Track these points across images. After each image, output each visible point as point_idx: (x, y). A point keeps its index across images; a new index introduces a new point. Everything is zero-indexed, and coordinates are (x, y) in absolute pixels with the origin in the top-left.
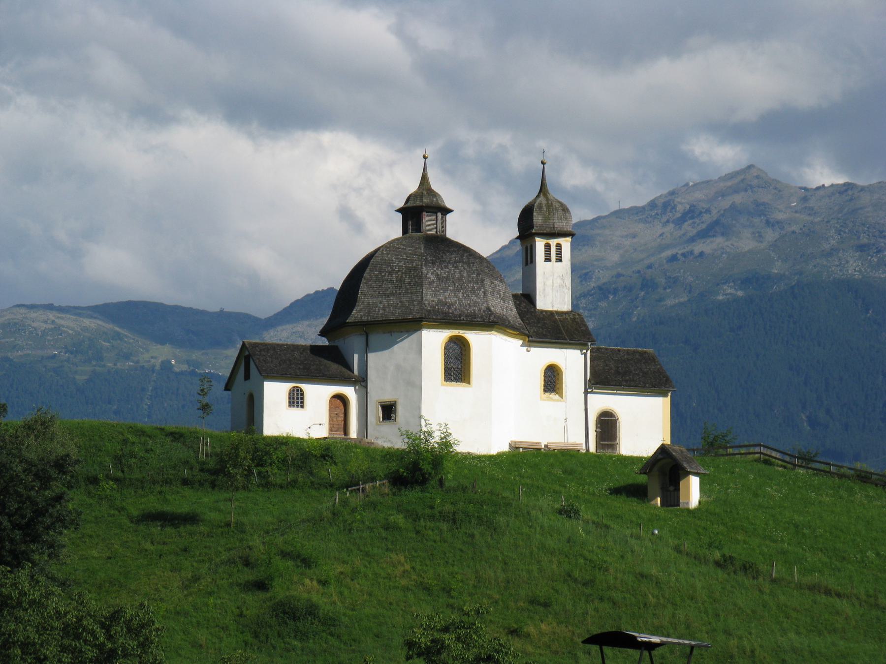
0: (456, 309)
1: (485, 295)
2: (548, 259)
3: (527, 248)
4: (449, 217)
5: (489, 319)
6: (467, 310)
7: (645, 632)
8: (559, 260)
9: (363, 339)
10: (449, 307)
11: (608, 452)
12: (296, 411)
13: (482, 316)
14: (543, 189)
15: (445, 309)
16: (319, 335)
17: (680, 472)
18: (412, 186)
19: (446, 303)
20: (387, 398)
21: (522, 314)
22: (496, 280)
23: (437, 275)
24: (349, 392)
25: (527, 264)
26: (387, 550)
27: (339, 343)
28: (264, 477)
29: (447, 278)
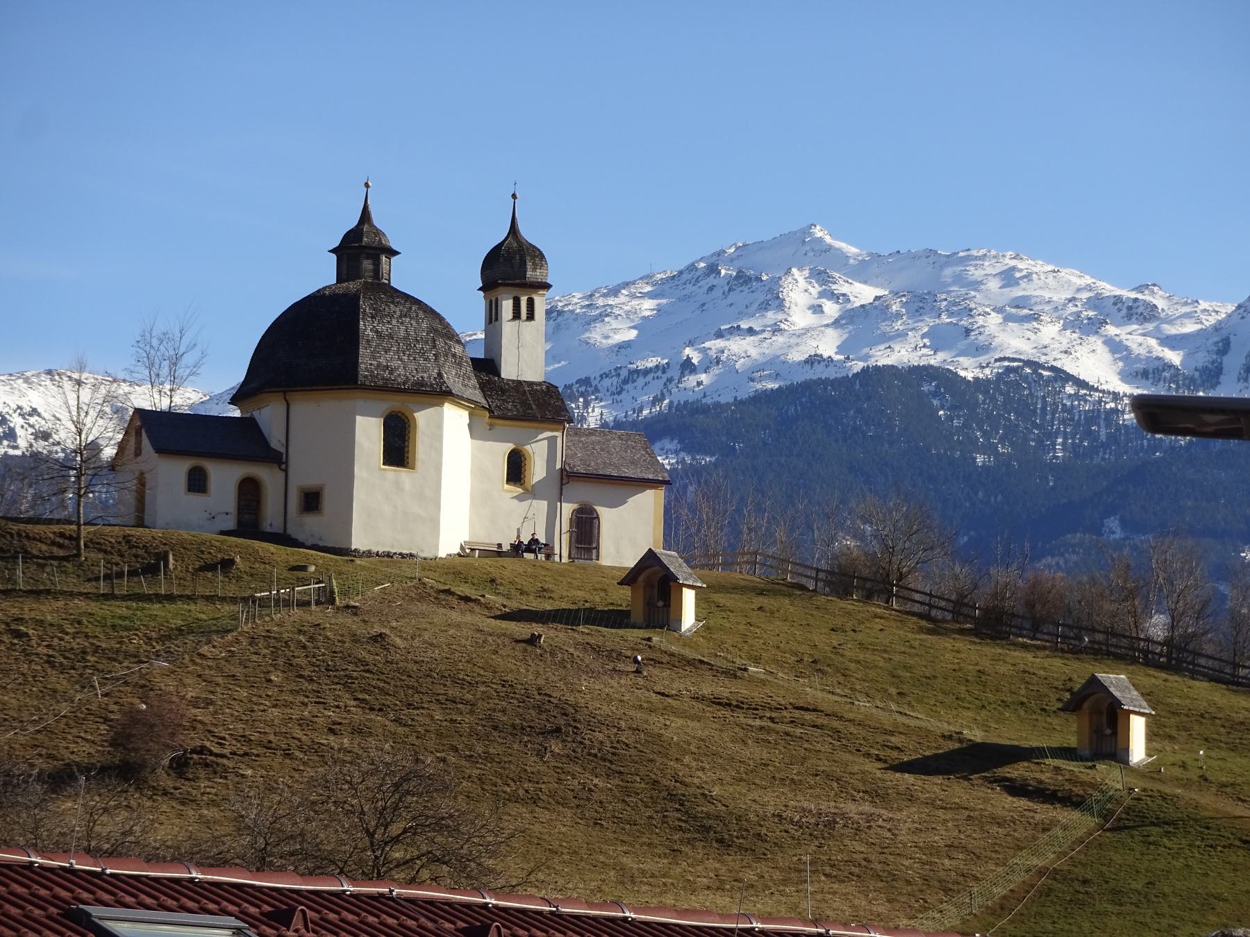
0: (399, 375)
1: (436, 359)
2: (516, 315)
3: (491, 301)
4: (394, 259)
5: (441, 388)
6: (413, 376)
7: (75, 769)
8: (531, 317)
9: (283, 408)
10: (391, 373)
11: (673, 561)
12: (196, 499)
13: (432, 385)
14: (365, 215)
15: (386, 375)
16: (229, 403)
17: (671, 583)
18: (499, 234)
19: (387, 367)
20: (311, 482)
21: (483, 387)
22: (451, 341)
23: (377, 332)
24: (264, 474)
25: (491, 322)
26: (914, 685)
27: (256, 414)
28: (62, 572)
29: (391, 336)
